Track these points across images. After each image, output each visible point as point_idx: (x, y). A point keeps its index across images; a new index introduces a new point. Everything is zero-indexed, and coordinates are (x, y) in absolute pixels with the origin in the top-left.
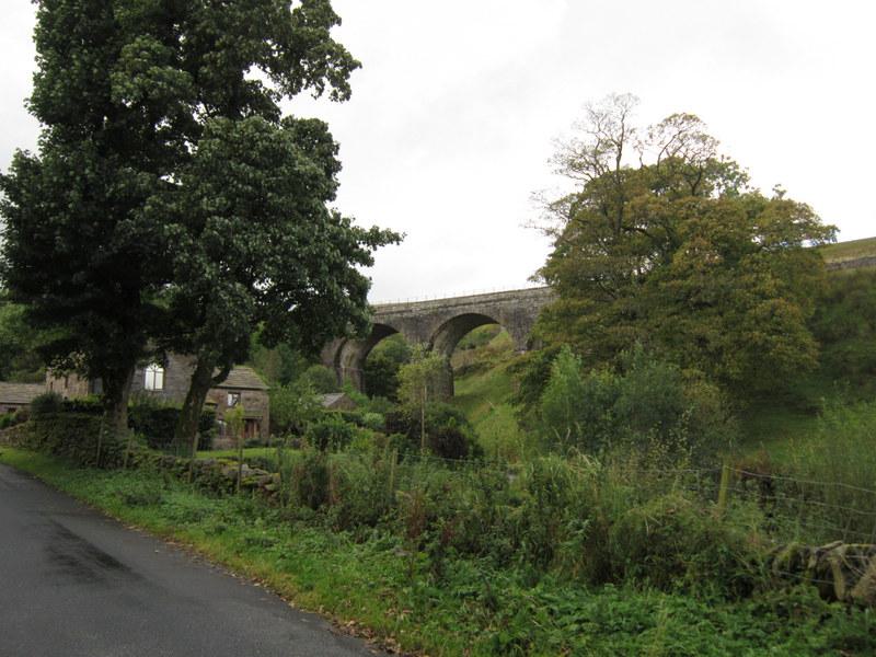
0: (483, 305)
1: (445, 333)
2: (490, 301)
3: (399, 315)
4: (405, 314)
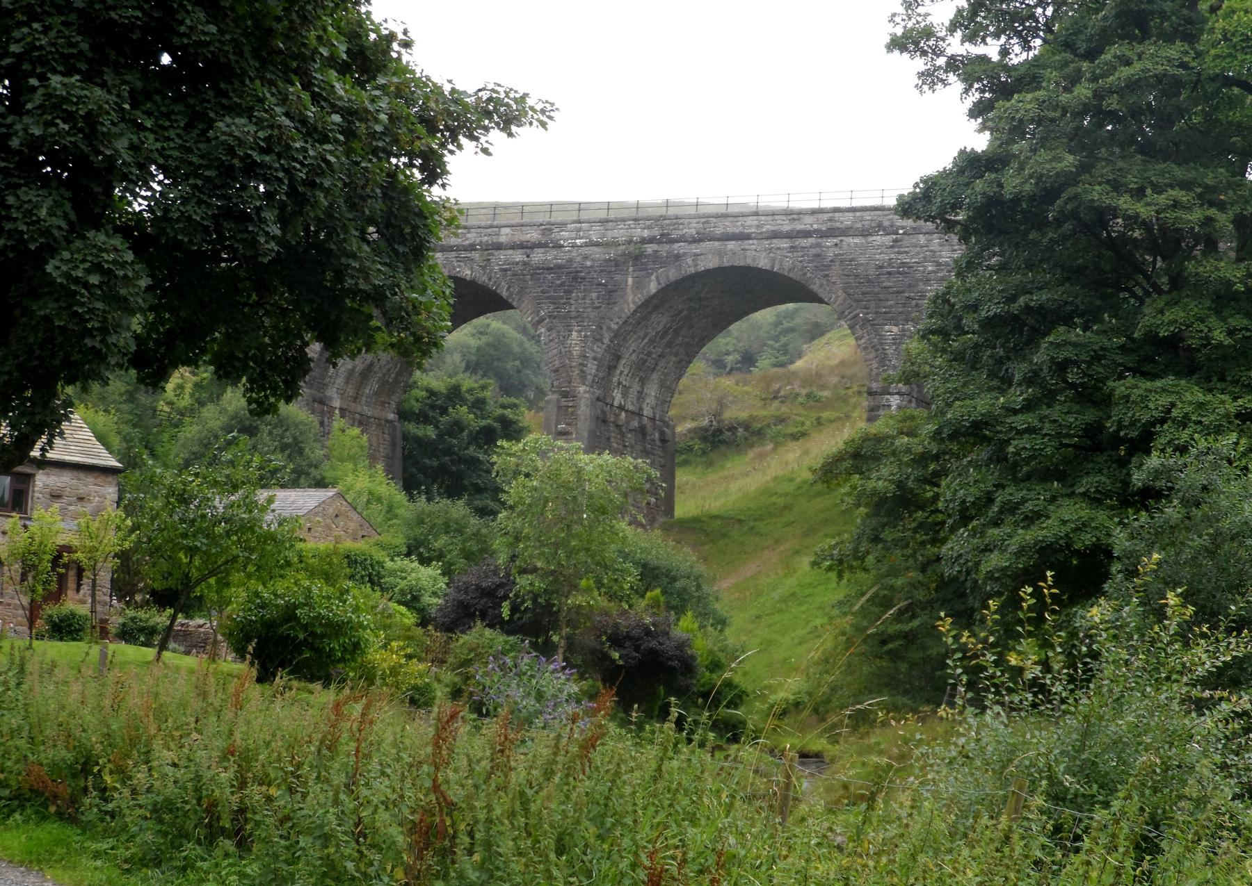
0: (785, 244)
1: (660, 321)
2: (806, 234)
3: (519, 256)
4: (538, 256)
